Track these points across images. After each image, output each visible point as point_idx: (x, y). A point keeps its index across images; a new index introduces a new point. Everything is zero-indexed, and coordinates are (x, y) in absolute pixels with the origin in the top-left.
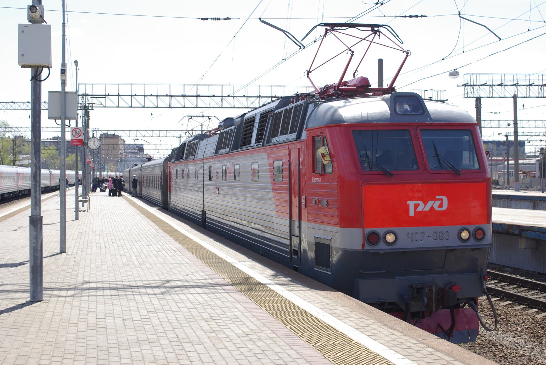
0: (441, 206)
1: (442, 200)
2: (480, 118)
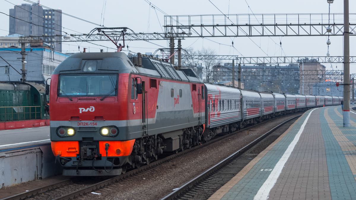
0: (92, 110)
1: (92, 108)
2: (205, 112)
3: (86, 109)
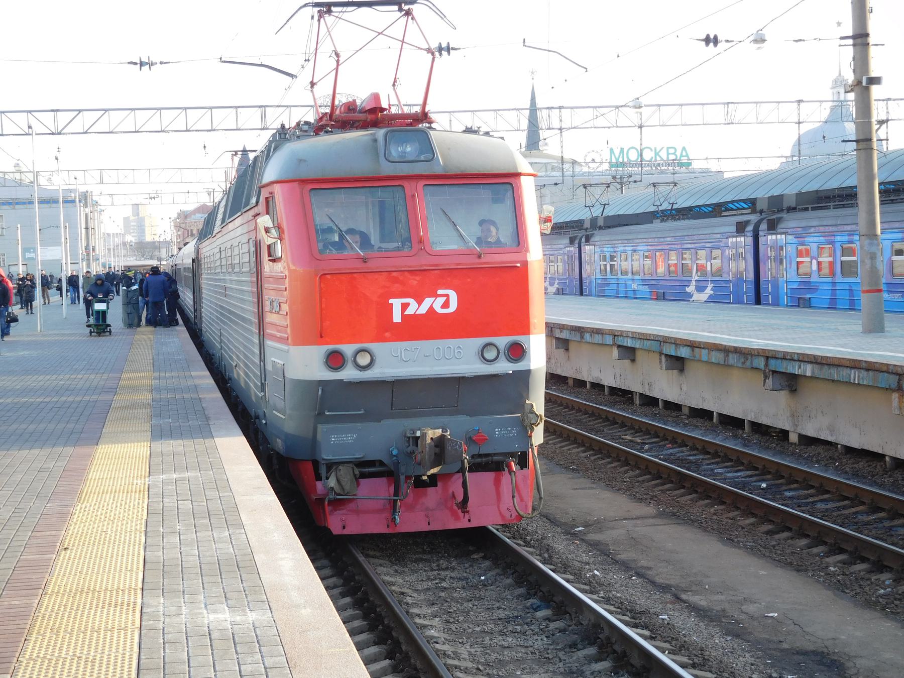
0: (446, 305)
1: (447, 296)
3: (420, 303)
